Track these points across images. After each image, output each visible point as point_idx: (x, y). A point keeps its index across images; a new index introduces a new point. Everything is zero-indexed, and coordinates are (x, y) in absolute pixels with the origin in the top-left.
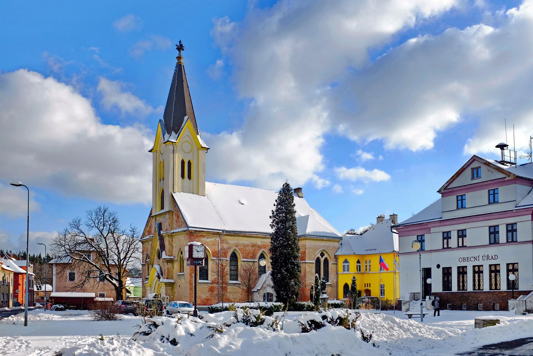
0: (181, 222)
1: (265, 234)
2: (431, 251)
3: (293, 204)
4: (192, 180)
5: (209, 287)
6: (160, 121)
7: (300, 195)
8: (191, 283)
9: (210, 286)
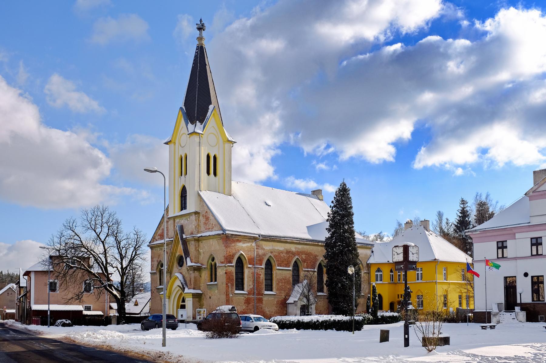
0: (213, 224)
1: (299, 240)
2: (515, 258)
3: (349, 206)
4: (217, 176)
5: (245, 299)
6: (181, 108)
7: (320, 197)
8: (227, 294)
9: (246, 297)
